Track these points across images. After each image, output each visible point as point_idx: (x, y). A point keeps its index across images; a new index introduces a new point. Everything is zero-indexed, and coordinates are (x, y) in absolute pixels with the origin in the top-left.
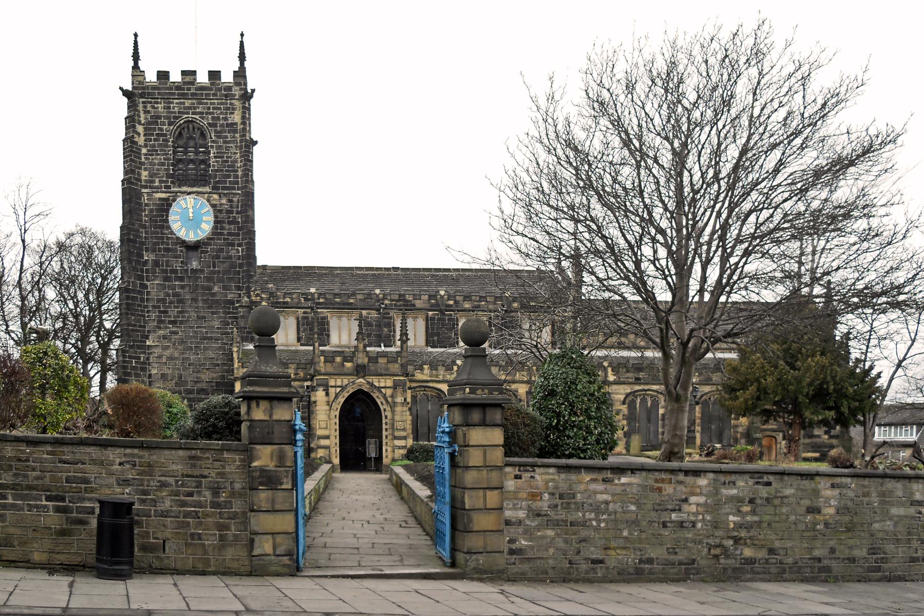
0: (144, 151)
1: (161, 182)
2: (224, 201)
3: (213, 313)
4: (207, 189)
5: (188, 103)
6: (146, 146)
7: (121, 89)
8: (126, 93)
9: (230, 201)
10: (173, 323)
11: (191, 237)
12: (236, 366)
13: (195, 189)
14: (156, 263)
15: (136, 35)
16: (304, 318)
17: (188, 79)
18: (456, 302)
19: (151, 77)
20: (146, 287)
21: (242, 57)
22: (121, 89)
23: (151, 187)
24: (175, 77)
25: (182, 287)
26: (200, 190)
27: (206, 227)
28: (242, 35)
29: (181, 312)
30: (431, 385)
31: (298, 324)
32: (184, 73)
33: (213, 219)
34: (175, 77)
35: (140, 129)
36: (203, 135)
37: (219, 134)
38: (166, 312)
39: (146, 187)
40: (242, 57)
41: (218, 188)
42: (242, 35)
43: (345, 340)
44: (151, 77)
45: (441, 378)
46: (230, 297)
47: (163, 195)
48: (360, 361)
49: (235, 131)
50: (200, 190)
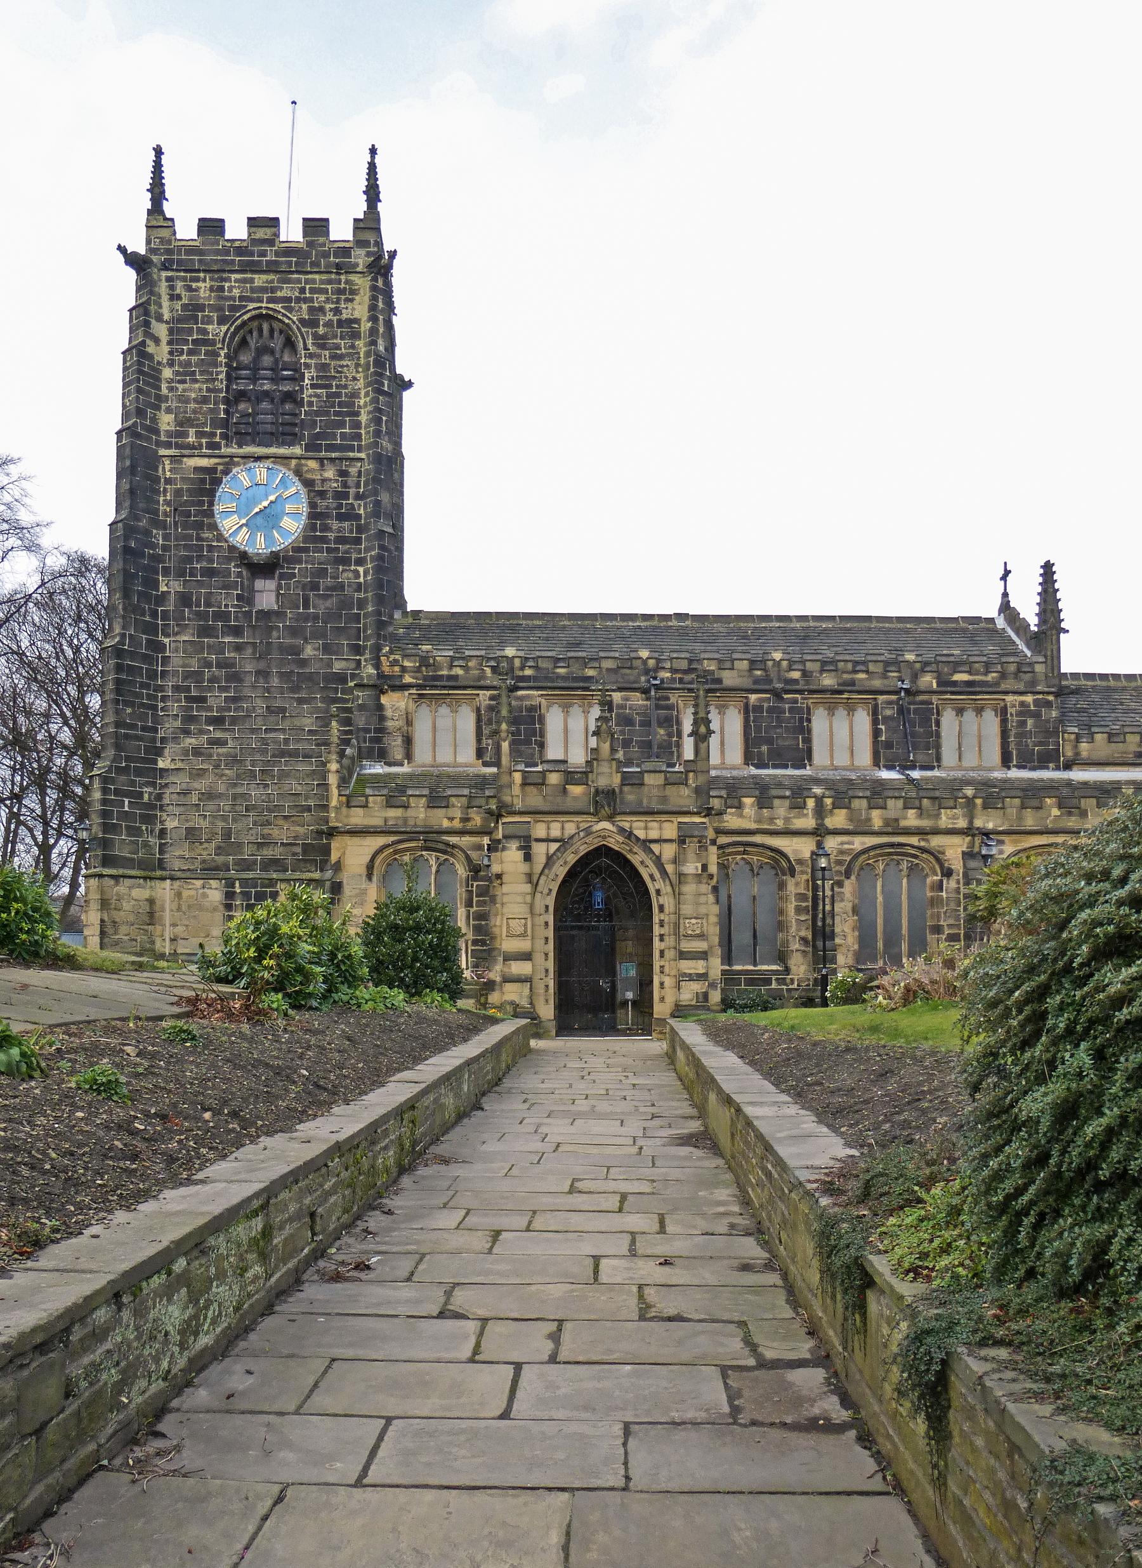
0: (167, 373)
1: (200, 434)
2: (330, 473)
3: (300, 701)
4: (297, 450)
5: (260, 280)
6: (171, 364)
7: (122, 249)
8: (132, 260)
9: (343, 473)
10: (217, 721)
11: (259, 546)
12: (334, 802)
13: (273, 450)
14: (185, 599)
15: (158, 151)
16: (491, 708)
17: (261, 233)
18: (805, 673)
19: (187, 231)
20: (161, 647)
21: (372, 193)
22: (122, 249)
23: (178, 446)
24: (292, 233)
25: (238, 648)
26: (282, 451)
27: (292, 526)
28: (373, 151)
29: (234, 699)
30: (758, 839)
31: (479, 720)
32: (253, 222)
33: (304, 509)
34: (236, 231)
35: (161, 330)
36: (290, 344)
37: (321, 342)
38: (203, 699)
39: (168, 445)
40: (372, 193)
41: (318, 448)
42: (373, 151)
43: (445, 756)
44: (187, 231)
45: (780, 824)
46: (338, 666)
47: (204, 462)
48: (602, 782)
49: (356, 335)
50: (282, 451)
